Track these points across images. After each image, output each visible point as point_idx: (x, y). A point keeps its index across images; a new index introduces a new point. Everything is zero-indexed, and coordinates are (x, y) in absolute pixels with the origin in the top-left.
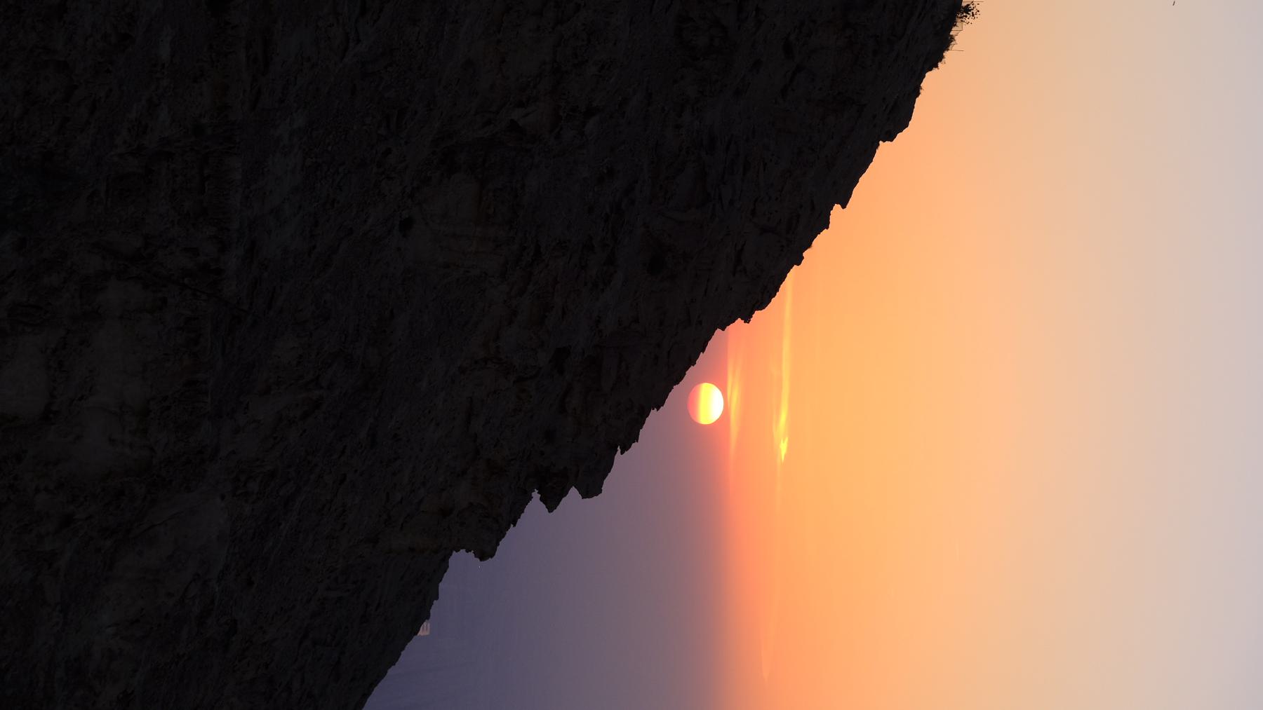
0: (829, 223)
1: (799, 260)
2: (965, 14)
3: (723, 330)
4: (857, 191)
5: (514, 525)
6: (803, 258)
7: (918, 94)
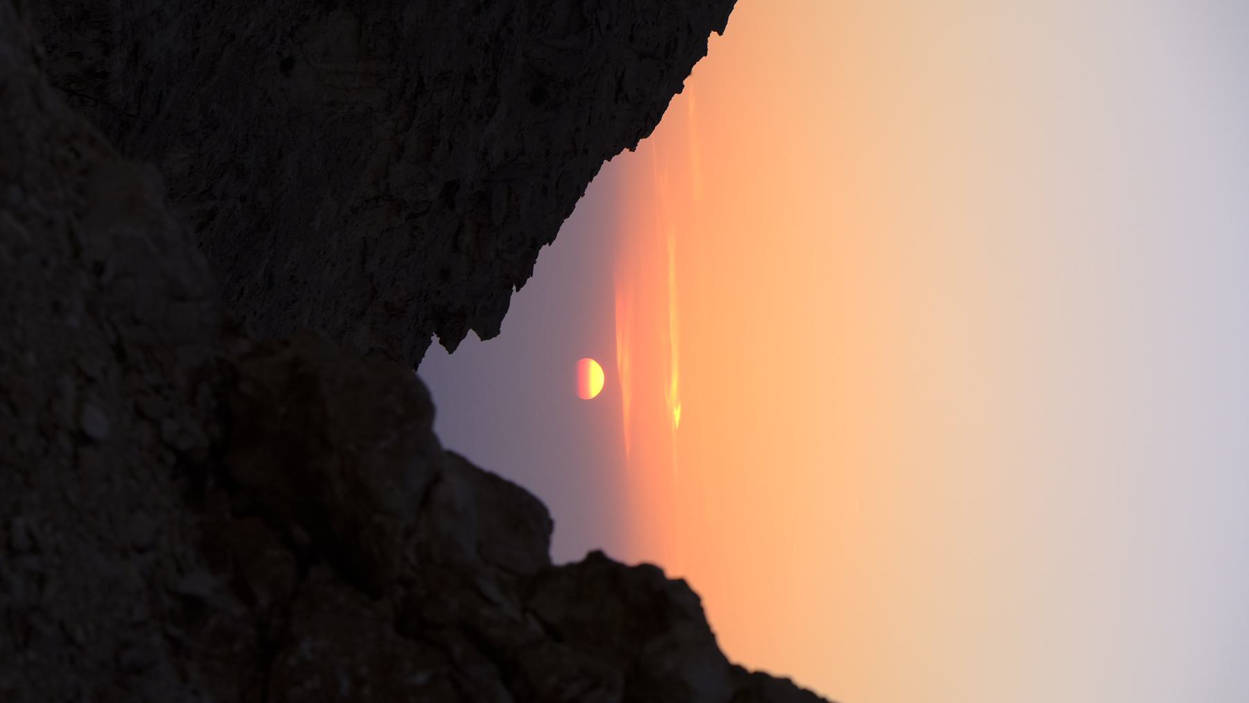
1: (679, 88)
6: (681, 584)
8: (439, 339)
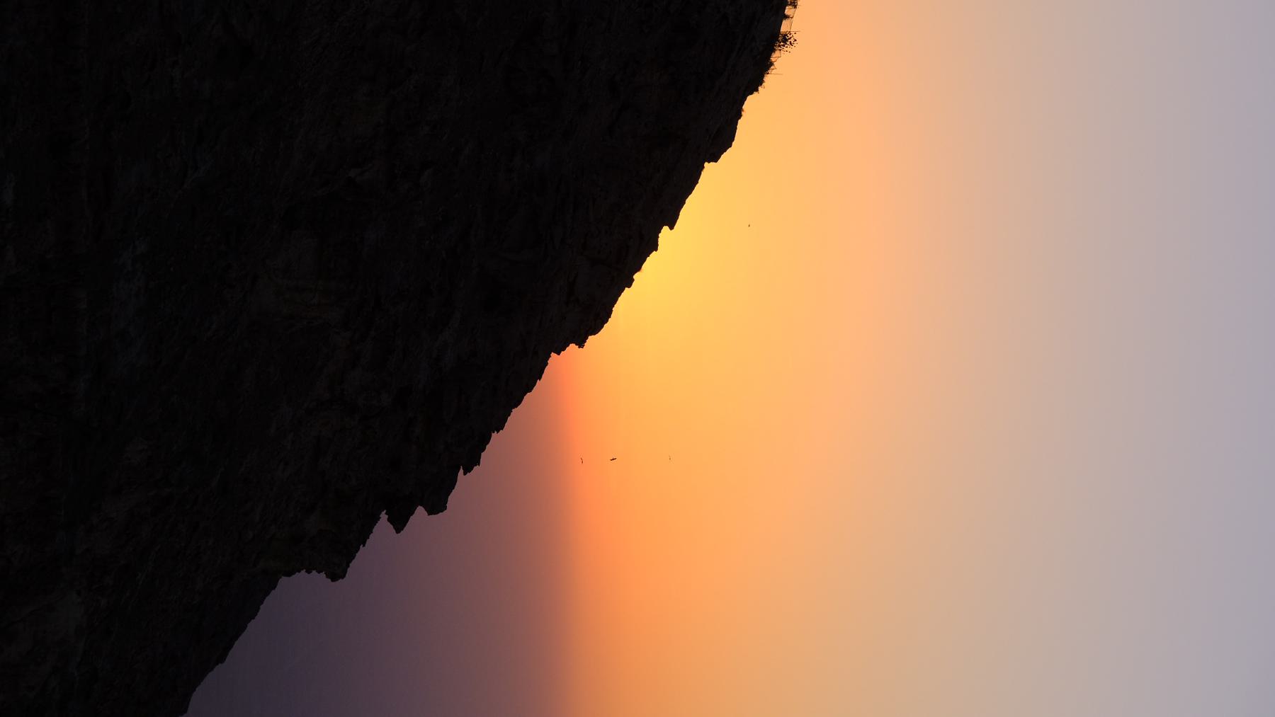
0: (658, 245)
1: (629, 283)
2: (782, 43)
3: (336, 575)
4: (683, 213)
5: (364, 546)
6: (633, 280)
7: (740, 116)
8: (314, 572)
